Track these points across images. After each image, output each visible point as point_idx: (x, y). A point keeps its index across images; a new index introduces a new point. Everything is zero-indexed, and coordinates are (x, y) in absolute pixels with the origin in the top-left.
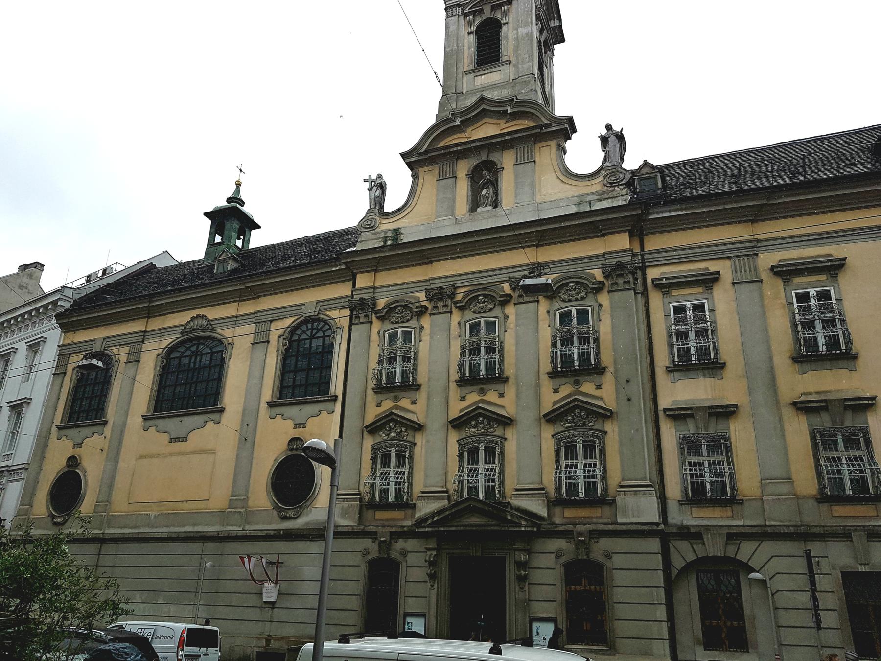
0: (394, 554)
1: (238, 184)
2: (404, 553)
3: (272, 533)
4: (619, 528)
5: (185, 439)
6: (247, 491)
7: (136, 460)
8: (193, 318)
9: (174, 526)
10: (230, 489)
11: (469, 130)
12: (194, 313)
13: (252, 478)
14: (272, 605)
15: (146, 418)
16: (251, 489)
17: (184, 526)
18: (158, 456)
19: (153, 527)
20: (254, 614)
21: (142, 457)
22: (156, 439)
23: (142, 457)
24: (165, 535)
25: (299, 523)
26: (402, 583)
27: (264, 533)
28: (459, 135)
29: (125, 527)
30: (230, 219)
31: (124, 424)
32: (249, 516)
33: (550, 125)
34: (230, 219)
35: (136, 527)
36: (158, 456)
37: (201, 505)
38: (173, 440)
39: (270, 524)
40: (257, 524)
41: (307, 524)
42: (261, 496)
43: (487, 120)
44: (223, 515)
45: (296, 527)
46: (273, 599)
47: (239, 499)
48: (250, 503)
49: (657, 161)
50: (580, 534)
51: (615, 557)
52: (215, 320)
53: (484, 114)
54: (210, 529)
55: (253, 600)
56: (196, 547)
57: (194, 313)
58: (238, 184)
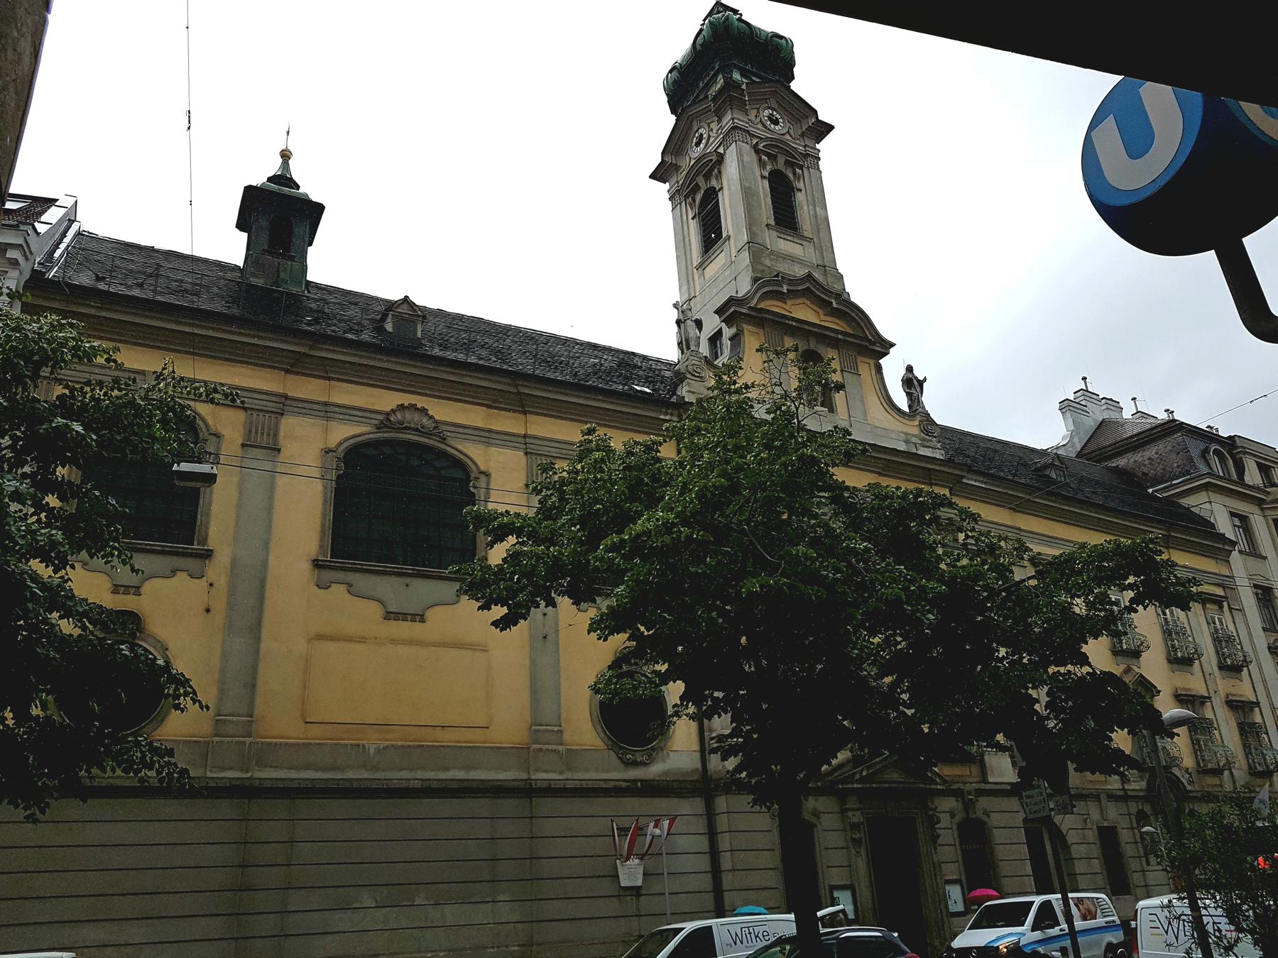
0: (979, 814)
1: (286, 155)
2: (816, 814)
3: (624, 785)
4: (988, 787)
5: (420, 618)
6: (559, 718)
7: (309, 642)
8: (401, 407)
9: (423, 768)
10: (527, 713)
11: (789, 302)
12: (407, 399)
13: (563, 698)
14: (636, 891)
15: (317, 564)
16: (563, 716)
17: (447, 769)
18: (362, 640)
19: (375, 768)
20: (611, 907)
21: (320, 637)
22: (353, 607)
23: (320, 637)
24: (417, 784)
25: (655, 770)
26: (777, 846)
27: (612, 784)
28: (779, 304)
29: (307, 767)
30: (278, 214)
31: (265, 564)
32: (571, 757)
33: (874, 344)
34: (278, 214)
35: (334, 768)
36: (362, 640)
37: (475, 736)
38: (390, 616)
39: (608, 771)
40: (587, 770)
41: (666, 773)
42: (583, 730)
43: (804, 300)
44: (522, 754)
45: (650, 777)
46: (639, 883)
47: (544, 730)
48: (567, 737)
49: (419, 300)
50: (969, 793)
51: (992, 815)
52: (447, 424)
53: (807, 293)
54: (502, 776)
55: (605, 887)
56: (480, 806)
57: (407, 399)
58: (286, 155)
